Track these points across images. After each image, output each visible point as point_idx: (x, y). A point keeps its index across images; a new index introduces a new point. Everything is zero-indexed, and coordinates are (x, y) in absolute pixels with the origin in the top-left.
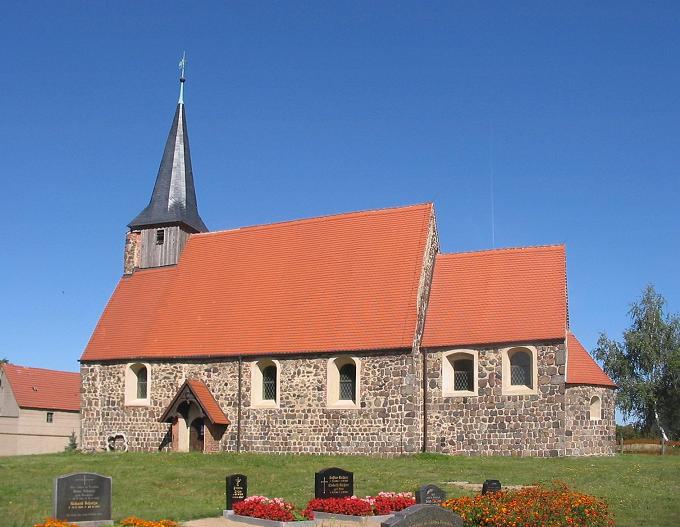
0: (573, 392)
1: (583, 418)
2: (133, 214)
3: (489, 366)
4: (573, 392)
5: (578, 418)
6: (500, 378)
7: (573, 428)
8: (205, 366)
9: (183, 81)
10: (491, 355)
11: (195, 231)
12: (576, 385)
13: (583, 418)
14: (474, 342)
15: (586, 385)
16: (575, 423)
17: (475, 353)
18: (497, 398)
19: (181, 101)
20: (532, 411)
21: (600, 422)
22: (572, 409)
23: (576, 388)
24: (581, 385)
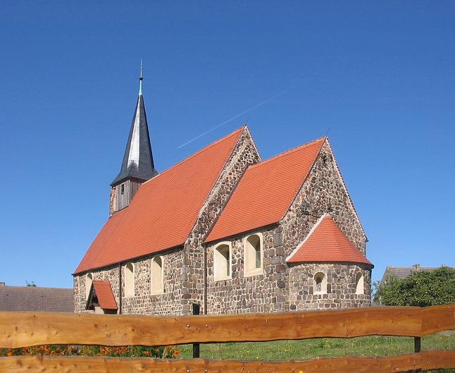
0: (297, 270)
1: (306, 293)
2: (114, 175)
3: (238, 253)
4: (297, 270)
5: (301, 293)
6: (242, 262)
7: (297, 303)
8: (110, 271)
9: (141, 79)
10: (238, 244)
11: (144, 181)
12: (299, 263)
13: (306, 293)
14: (359, 261)
15: (308, 262)
16: (299, 298)
17: (229, 243)
18: (242, 279)
19: (140, 94)
20: (261, 288)
21: (325, 296)
22: (295, 285)
23: (299, 267)
24: (304, 263)
